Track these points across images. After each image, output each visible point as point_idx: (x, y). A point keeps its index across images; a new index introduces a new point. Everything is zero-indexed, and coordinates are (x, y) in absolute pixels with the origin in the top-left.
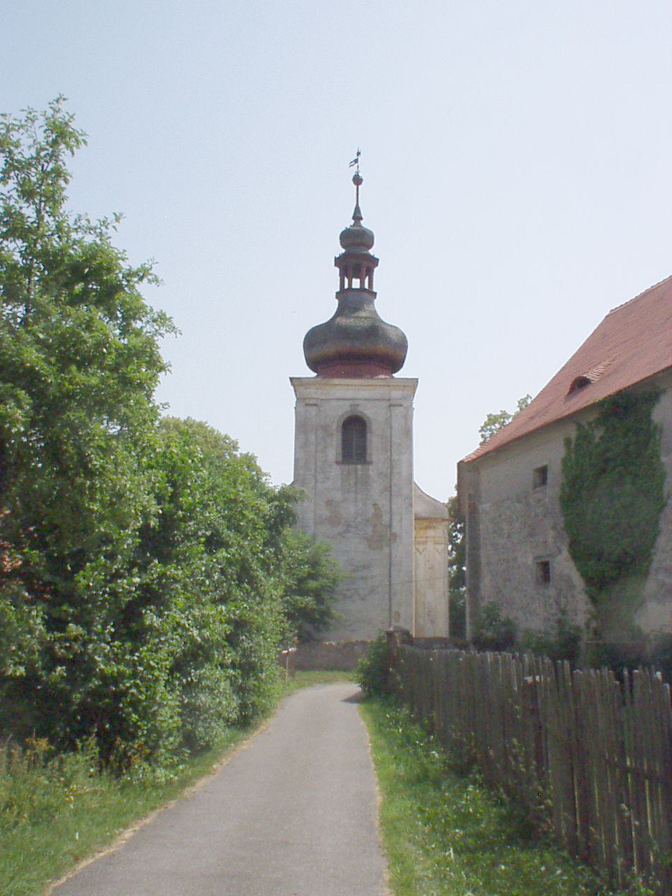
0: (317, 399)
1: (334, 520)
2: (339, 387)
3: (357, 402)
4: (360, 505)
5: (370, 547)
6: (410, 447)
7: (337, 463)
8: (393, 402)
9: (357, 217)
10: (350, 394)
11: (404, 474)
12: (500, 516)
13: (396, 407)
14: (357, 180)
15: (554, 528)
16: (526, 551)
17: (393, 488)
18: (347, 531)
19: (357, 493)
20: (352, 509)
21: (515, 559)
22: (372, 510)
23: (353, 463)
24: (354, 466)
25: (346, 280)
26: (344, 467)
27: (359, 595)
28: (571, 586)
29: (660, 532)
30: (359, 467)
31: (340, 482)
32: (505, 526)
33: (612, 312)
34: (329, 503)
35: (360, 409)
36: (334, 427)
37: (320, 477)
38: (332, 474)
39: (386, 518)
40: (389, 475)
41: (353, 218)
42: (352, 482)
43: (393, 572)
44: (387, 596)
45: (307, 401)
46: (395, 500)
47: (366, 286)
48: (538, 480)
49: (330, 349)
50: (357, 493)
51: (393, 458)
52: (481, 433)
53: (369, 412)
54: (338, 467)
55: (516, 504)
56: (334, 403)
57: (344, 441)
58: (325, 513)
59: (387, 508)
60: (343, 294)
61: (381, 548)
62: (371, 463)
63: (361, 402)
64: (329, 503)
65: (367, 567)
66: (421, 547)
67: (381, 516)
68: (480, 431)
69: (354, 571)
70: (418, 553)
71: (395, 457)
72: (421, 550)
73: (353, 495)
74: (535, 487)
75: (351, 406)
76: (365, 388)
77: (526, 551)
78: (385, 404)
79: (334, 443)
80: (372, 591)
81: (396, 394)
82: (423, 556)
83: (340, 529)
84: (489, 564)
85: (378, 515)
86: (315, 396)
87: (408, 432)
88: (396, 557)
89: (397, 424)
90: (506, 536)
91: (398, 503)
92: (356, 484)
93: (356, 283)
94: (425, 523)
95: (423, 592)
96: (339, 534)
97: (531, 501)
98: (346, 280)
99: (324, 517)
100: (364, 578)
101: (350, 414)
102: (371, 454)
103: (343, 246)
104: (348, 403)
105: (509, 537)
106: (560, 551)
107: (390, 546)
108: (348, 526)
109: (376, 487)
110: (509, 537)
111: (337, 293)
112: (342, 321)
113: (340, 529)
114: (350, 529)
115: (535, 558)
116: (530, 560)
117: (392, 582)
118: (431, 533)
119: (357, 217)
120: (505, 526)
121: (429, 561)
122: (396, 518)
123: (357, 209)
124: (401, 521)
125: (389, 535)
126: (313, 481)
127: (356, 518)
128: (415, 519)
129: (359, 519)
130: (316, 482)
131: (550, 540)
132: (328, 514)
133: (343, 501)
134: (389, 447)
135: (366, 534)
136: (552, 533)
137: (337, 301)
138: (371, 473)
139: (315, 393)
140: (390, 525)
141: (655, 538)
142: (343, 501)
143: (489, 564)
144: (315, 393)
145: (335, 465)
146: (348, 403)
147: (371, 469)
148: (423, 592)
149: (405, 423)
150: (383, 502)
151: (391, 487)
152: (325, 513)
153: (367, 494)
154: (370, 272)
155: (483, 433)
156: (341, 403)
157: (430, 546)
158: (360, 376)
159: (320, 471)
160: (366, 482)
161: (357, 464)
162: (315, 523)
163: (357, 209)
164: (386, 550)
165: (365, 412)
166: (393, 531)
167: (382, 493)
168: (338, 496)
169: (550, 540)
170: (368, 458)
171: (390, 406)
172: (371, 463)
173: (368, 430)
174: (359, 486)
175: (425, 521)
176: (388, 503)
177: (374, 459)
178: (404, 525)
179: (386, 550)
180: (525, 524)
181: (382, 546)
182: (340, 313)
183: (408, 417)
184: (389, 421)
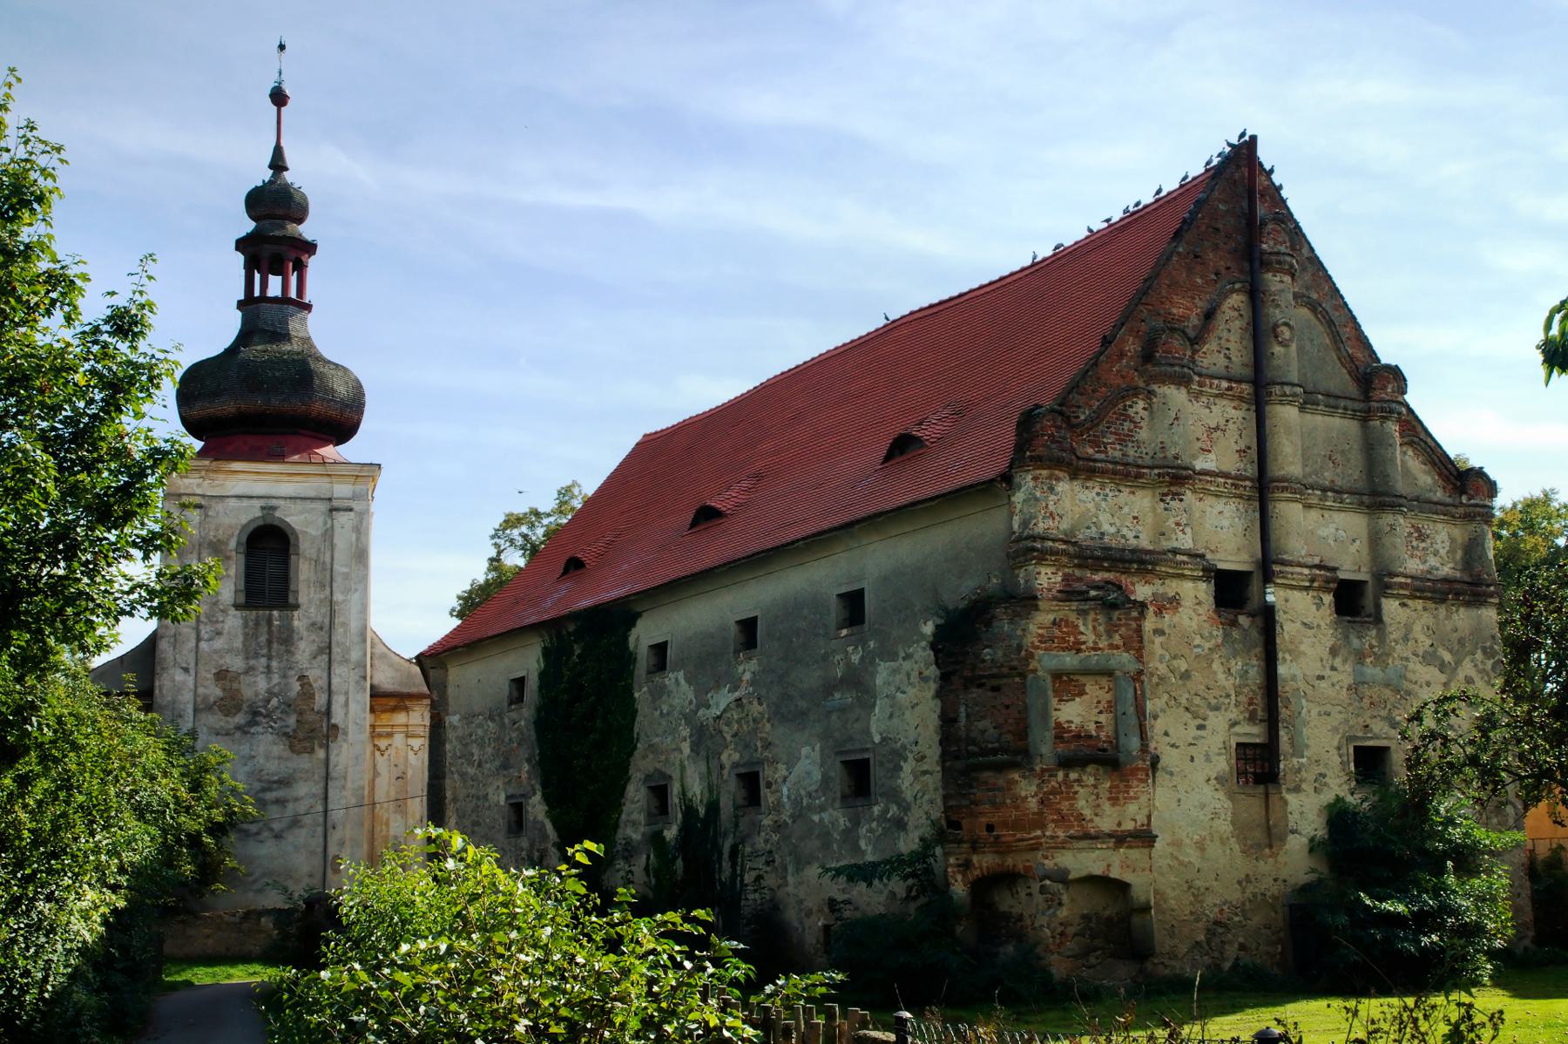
0: (203, 496)
1: (229, 703)
2: (241, 476)
3: (274, 502)
4: (276, 679)
5: (292, 748)
6: (364, 579)
7: (237, 606)
8: (335, 503)
9: (278, 163)
10: (260, 488)
11: (354, 625)
12: (471, 736)
13: (342, 513)
14: (279, 98)
15: (529, 761)
16: (498, 787)
17: (335, 649)
18: (252, 723)
19: (270, 658)
20: (262, 684)
21: (486, 797)
22: (296, 687)
23: (264, 608)
24: (268, 612)
25: (257, 276)
26: (248, 612)
27: (271, 830)
28: (545, 837)
29: (629, 779)
30: (275, 613)
31: (241, 638)
32: (475, 750)
33: (647, 439)
34: (222, 675)
35: (278, 514)
36: (233, 544)
37: (205, 631)
38: (226, 627)
39: (320, 700)
40: (327, 627)
41: (271, 167)
42: (263, 639)
43: (331, 793)
44: (320, 830)
45: (185, 499)
46: (338, 670)
47: (293, 294)
48: (515, 694)
49: (227, 407)
50: (270, 658)
51: (335, 598)
52: (493, 541)
53: (295, 518)
54: (238, 613)
55: (490, 723)
56: (233, 503)
57: (248, 567)
58: (214, 691)
59: (323, 683)
60: (248, 304)
61: (312, 751)
62: (296, 607)
63: (282, 502)
64: (222, 675)
65: (285, 782)
66: (383, 743)
67: (312, 696)
68: (493, 537)
69: (263, 790)
70: (377, 753)
71: (338, 597)
72: (383, 748)
73: (263, 661)
74: (511, 704)
75: (263, 508)
76: (286, 478)
77: (498, 787)
78: (322, 507)
79: (232, 572)
80: (295, 823)
81: (342, 490)
82: (386, 756)
83: (240, 719)
84: (455, 800)
85: (307, 693)
86: (199, 491)
87: (361, 556)
88: (336, 766)
89: (343, 539)
90: (476, 763)
91: (343, 676)
92: (269, 642)
93: (275, 286)
94: (392, 702)
95: (385, 819)
96: (238, 728)
97: (506, 721)
98: (257, 276)
99: (212, 700)
100: (281, 802)
101: (261, 523)
102: (297, 592)
103: (252, 218)
104: (258, 503)
105: (480, 765)
106: (534, 794)
107: (327, 748)
108: (256, 713)
109: (304, 650)
110: (480, 765)
111: (239, 302)
112: (246, 353)
113: (240, 719)
114: (258, 719)
115: (508, 797)
116: (502, 797)
117: (330, 806)
118: (401, 718)
119: (278, 163)
120: (475, 750)
121: (396, 766)
122: (338, 700)
123: (278, 153)
124: (346, 704)
125: (325, 729)
126: (193, 636)
127: (268, 701)
128: (371, 696)
129: (274, 702)
130: (198, 639)
131: (524, 775)
132: (218, 692)
133: (246, 672)
134: (327, 580)
135: (287, 726)
136: (526, 767)
137: (239, 314)
138: (296, 623)
139: (199, 485)
140: (328, 713)
141: (626, 783)
142: (246, 672)
143: (455, 800)
144: (199, 485)
145: (232, 611)
146: (258, 503)
147: (296, 616)
148: (385, 819)
149: (358, 539)
150: (316, 674)
151: (330, 647)
152: (214, 691)
153: (288, 660)
154: (300, 267)
155: (498, 541)
156: (245, 503)
157: (398, 739)
158: (278, 457)
159: (205, 620)
160: (287, 639)
161: (272, 608)
162: (196, 710)
163: (278, 153)
164: (321, 754)
165: (288, 520)
166: (333, 721)
167: (315, 658)
168: (236, 663)
169: (524, 775)
170: (291, 600)
171: (332, 510)
172: (296, 607)
173: (291, 550)
174: (275, 646)
175: (384, 700)
176: (325, 675)
177: (302, 599)
178: (352, 711)
179: (321, 754)
180: (499, 749)
181: (313, 749)
182: (244, 337)
183: (361, 530)
184: (328, 535)
